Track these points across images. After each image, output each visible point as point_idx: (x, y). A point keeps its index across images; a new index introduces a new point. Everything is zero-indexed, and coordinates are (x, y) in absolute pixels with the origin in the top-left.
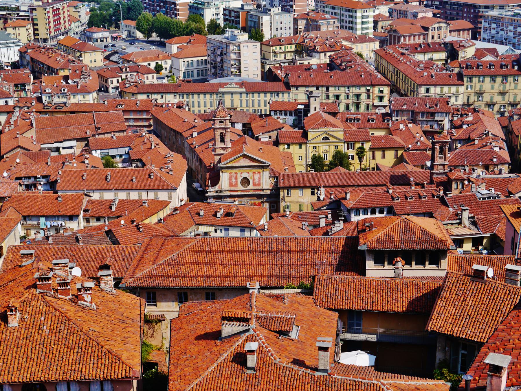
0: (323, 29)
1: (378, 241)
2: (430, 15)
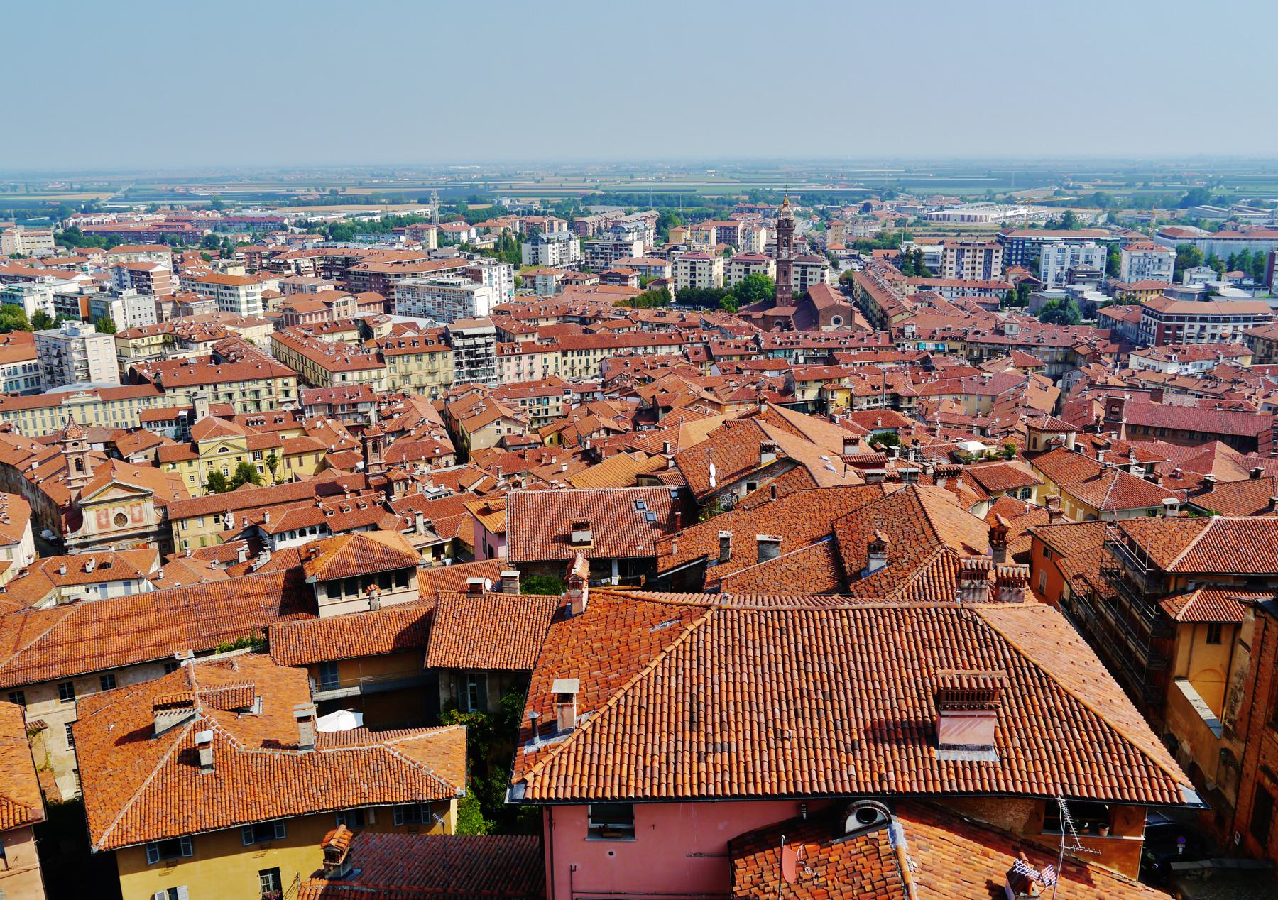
0: (197, 312)
1: (329, 569)
2: (332, 288)
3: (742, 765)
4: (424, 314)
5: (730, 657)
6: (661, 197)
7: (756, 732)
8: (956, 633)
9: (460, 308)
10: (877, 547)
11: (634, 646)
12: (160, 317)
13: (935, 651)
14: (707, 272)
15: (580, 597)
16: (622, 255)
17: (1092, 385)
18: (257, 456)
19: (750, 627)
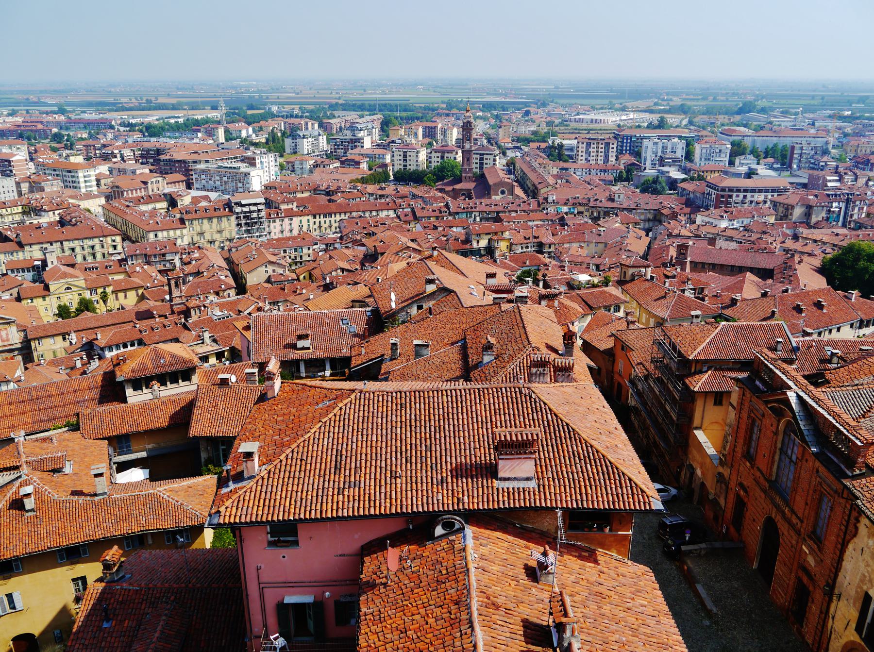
0: (47, 189)
1: (133, 371)
2: (147, 171)
3: (367, 496)
4: (214, 189)
5: (365, 424)
6: (385, 105)
7: (378, 474)
8: (517, 404)
9: (240, 185)
10: (488, 347)
11: (303, 418)
12: (20, 193)
13: (503, 416)
14: (414, 158)
15: (272, 386)
16: (356, 146)
17: (670, 235)
18: (93, 292)
19: (381, 403)
